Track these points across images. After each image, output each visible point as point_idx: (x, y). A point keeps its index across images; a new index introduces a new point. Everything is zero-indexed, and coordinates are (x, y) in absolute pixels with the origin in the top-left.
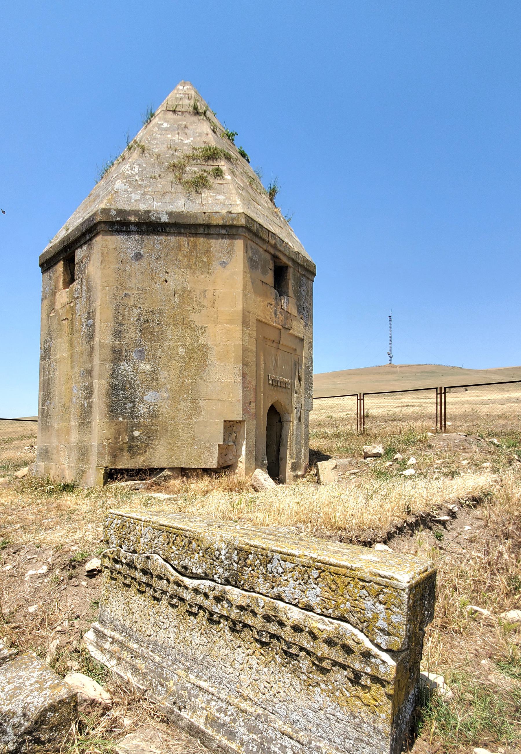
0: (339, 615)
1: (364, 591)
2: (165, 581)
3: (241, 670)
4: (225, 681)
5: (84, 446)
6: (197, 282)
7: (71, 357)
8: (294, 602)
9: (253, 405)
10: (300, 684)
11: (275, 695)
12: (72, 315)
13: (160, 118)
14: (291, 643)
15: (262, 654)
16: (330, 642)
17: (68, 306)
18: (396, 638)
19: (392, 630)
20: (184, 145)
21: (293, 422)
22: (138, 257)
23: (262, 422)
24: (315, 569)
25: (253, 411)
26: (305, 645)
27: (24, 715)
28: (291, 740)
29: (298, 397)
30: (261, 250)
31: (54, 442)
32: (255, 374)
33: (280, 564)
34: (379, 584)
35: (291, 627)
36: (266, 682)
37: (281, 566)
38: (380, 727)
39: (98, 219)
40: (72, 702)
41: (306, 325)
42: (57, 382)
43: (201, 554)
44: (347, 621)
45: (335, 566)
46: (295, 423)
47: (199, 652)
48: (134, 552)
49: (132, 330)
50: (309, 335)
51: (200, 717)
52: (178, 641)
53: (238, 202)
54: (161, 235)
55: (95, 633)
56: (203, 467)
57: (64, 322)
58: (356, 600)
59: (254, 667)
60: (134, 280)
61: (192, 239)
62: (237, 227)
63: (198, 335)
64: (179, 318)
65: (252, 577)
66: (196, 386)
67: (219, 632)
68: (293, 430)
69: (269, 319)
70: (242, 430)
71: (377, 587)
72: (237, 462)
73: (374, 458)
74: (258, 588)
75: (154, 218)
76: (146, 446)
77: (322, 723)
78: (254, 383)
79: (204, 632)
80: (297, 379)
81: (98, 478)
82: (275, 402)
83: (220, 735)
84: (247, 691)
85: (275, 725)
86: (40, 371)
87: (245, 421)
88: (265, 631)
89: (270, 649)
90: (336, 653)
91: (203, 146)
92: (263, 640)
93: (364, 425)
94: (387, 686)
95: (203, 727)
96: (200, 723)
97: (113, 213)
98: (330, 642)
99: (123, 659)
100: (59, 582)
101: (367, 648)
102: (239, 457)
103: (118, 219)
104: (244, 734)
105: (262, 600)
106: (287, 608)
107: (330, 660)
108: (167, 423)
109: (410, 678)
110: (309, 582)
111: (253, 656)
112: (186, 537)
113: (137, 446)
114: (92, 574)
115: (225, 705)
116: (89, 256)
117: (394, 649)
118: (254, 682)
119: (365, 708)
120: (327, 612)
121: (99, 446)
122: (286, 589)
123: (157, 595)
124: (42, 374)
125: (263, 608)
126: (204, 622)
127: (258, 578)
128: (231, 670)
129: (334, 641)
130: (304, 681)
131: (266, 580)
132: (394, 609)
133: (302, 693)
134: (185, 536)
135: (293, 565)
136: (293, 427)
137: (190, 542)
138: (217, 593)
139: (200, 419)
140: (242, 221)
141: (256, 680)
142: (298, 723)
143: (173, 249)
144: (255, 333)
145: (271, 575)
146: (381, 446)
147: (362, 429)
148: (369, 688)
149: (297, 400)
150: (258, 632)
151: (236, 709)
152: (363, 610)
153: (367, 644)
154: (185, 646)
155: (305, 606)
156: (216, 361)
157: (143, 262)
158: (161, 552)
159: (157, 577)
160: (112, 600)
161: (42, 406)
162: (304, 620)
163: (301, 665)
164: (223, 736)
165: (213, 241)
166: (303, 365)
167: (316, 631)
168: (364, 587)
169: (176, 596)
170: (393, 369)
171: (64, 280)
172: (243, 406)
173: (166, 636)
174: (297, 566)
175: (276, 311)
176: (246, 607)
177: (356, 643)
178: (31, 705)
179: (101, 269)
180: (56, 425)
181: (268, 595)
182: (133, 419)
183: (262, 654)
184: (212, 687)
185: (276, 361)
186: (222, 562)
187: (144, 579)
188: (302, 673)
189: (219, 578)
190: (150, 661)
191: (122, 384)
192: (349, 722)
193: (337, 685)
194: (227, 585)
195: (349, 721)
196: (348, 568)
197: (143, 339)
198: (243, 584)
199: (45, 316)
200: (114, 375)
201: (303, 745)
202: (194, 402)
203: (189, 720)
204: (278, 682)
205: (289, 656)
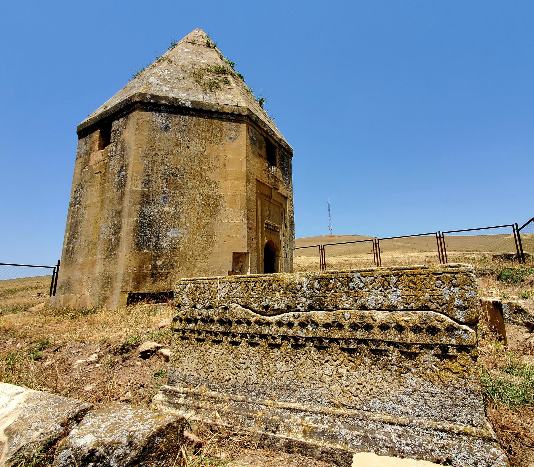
2: (245, 325)
3: (331, 382)
4: (315, 397)
5: (109, 275)
6: (213, 150)
7: (102, 202)
8: (378, 307)
11: (368, 393)
12: (106, 169)
13: (182, 46)
15: (351, 361)
16: (416, 329)
17: (102, 163)
19: (468, 304)
20: (200, 63)
22: (167, 129)
25: (254, 246)
26: (393, 339)
27: (130, 444)
28: (393, 426)
29: (285, 239)
30: (258, 133)
31: (78, 274)
33: (361, 280)
34: (450, 273)
35: (379, 327)
38: (472, 387)
39: (136, 99)
40: (180, 427)
41: (288, 188)
42: (85, 223)
43: (282, 292)
45: (411, 269)
47: (285, 379)
48: (210, 307)
52: (261, 376)
53: (242, 100)
54: (186, 115)
55: (165, 394)
57: (97, 175)
58: (434, 290)
59: (344, 375)
60: (162, 145)
61: (209, 120)
62: (242, 116)
64: (198, 174)
67: (305, 354)
69: (265, 180)
71: (449, 275)
75: (180, 104)
76: (168, 273)
77: (418, 403)
78: (255, 224)
80: (283, 225)
81: (121, 301)
84: (338, 399)
86: (69, 215)
88: (352, 339)
89: (358, 354)
91: (215, 65)
92: (351, 347)
95: (303, 440)
97: (148, 96)
98: (416, 329)
99: (202, 408)
100: (112, 365)
103: (152, 101)
104: (347, 434)
107: (418, 344)
110: (389, 287)
112: (265, 281)
114: (145, 355)
115: (319, 416)
116: (125, 126)
118: (345, 388)
123: (237, 339)
124: (70, 218)
125: (349, 319)
126: (289, 350)
127: (341, 297)
131: (349, 296)
132: (467, 288)
137: (270, 285)
138: (302, 319)
139: (214, 251)
140: (246, 112)
142: (395, 410)
143: (194, 125)
144: (255, 188)
145: (353, 291)
150: (345, 342)
152: (441, 296)
154: (269, 378)
155: (389, 307)
157: (171, 133)
158: (239, 301)
159: (236, 322)
160: (184, 358)
161: (68, 244)
163: (390, 358)
164: (326, 442)
165: (224, 123)
167: (403, 323)
168: (438, 279)
169: (258, 335)
170: (333, 238)
171: (100, 144)
173: (250, 373)
175: (268, 175)
178: (137, 433)
179: (136, 134)
180: (80, 260)
183: (351, 361)
185: (269, 211)
186: (304, 293)
187: (221, 329)
189: (302, 307)
190: (232, 402)
191: (149, 222)
192: (442, 393)
195: (443, 392)
199: (78, 171)
200: (142, 215)
201: (404, 426)
202: (209, 237)
203: (287, 439)
204: (369, 381)
205: (378, 354)
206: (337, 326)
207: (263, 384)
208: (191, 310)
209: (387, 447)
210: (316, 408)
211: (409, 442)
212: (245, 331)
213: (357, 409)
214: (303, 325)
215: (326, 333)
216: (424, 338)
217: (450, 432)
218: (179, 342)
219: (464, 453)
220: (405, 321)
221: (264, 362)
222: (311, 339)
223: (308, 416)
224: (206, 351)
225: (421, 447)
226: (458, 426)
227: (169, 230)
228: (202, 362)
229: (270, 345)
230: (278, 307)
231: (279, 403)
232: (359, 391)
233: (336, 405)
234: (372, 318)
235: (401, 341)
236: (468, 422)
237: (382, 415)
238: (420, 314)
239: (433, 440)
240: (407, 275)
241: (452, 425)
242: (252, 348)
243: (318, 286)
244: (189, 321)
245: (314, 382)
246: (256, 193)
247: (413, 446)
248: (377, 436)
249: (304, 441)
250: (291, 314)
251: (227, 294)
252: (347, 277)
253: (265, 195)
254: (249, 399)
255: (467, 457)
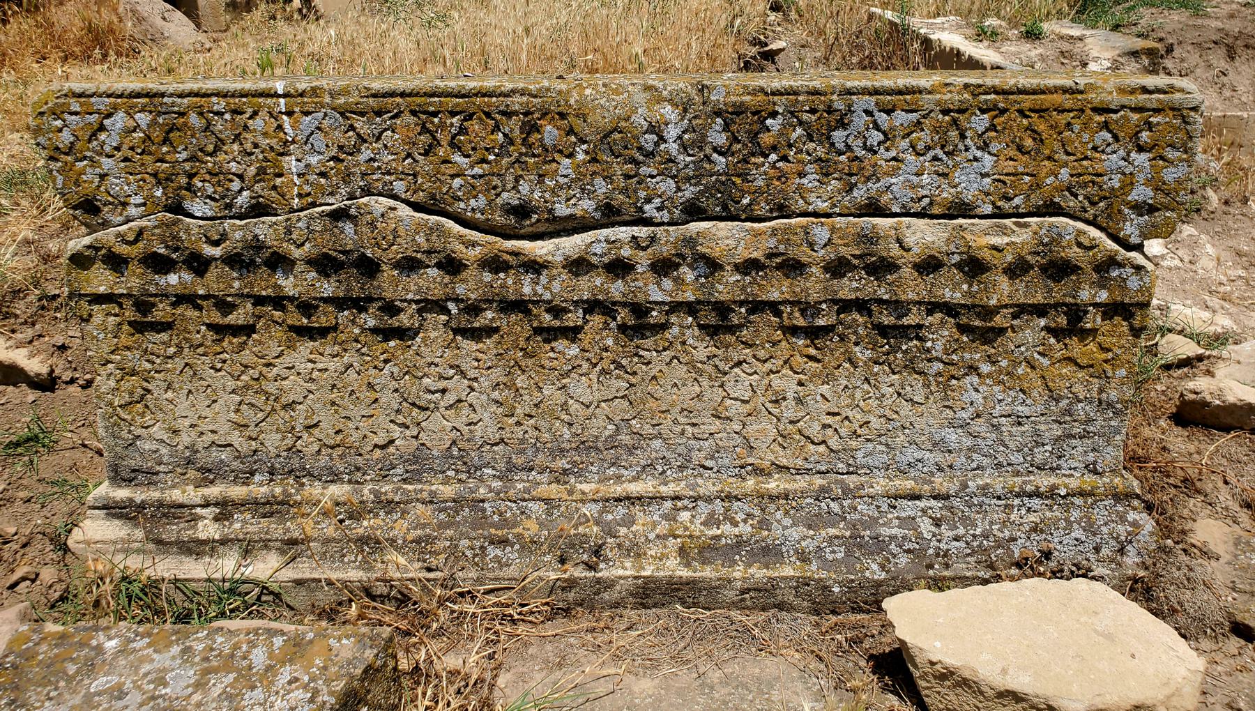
2: (433, 272)
3: (750, 415)
4: (697, 457)
8: (917, 208)
16: (1017, 270)
28: (917, 502)
34: (1138, 109)
43: (581, 157)
45: (1034, 92)
47: (599, 422)
48: (259, 210)
58: (1086, 158)
59: (790, 395)
65: (779, 179)
67: (665, 349)
74: (801, 201)
83: (741, 568)
84: (766, 455)
89: (836, 338)
95: (684, 573)
96: (674, 568)
98: (1017, 270)
112: (508, 114)
115: (718, 506)
118: (790, 427)
123: (405, 320)
126: (610, 342)
127: (801, 175)
131: (827, 175)
132: (1171, 154)
134: (503, 113)
135: (914, 117)
137: (531, 128)
138: (664, 249)
142: (920, 465)
145: (843, 158)
150: (803, 312)
152: (1101, 175)
154: (544, 425)
155: (949, 209)
158: (399, 187)
159: (397, 265)
163: (929, 344)
164: (750, 566)
167: (986, 255)
168: (1106, 126)
169: (490, 302)
176: (762, 259)
187: (328, 288)
194: (688, 222)
203: (636, 578)
204: (862, 403)
206: (779, 267)
207: (522, 441)
208: (162, 224)
209: (909, 551)
210: (707, 486)
211: (961, 531)
212: (438, 293)
213: (819, 472)
214: (663, 267)
215: (743, 288)
216: (1033, 291)
217: (1051, 493)
218: (124, 340)
219: (1078, 533)
220: (995, 248)
221: (521, 381)
222: (692, 308)
223: (686, 508)
224: (268, 365)
225: (987, 538)
226: (1067, 480)
228: (259, 400)
229: (538, 331)
230: (569, 211)
231: (585, 487)
232: (829, 432)
233: (762, 470)
234: (899, 241)
235: (969, 301)
236: (1086, 467)
237: (891, 480)
238: (1035, 227)
239: (1013, 517)
240: (1021, 112)
241: (1053, 480)
242: (469, 345)
243: (721, 139)
244: (160, 264)
245: (694, 421)
247: (970, 538)
248: (885, 531)
249: (690, 574)
250: (623, 233)
251: (335, 159)
252: (830, 110)
254: (482, 491)
255: (1083, 538)
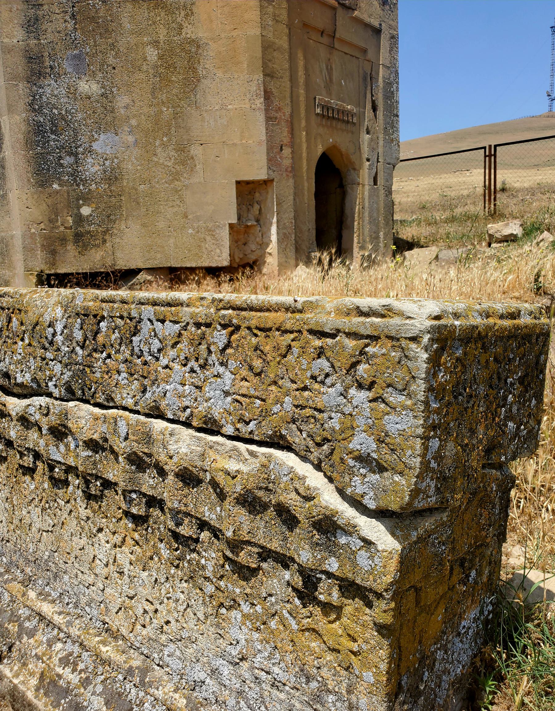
0: (270, 433)
1: (323, 363)
3: (106, 578)
9: (287, 151)
10: (204, 603)
14: (179, 512)
16: (251, 503)
18: (397, 478)
19: (388, 458)
21: (363, 185)
23: (306, 184)
24: (219, 327)
25: (287, 162)
29: (371, 140)
32: (288, 94)
33: (154, 330)
34: (353, 335)
35: (177, 475)
36: (147, 600)
37: (156, 335)
43: (27, 341)
44: (288, 448)
45: (260, 310)
46: (367, 187)
47: (41, 546)
49: (58, 17)
50: (391, 22)
51: (32, 674)
52: (12, 527)
56: (206, 264)
58: (305, 388)
63: (179, 20)
66: (183, 120)
68: (363, 199)
70: (269, 196)
71: (350, 343)
72: (263, 256)
73: (505, 244)
76: (105, 233)
78: (287, 110)
79: (47, 505)
80: (369, 106)
82: (329, 149)
84: (118, 622)
85: (156, 692)
87: (273, 180)
88: (135, 491)
90: (265, 527)
92: (134, 511)
93: (495, 200)
94: (375, 603)
95: (30, 695)
101: (326, 508)
102: (267, 245)
105: (126, 420)
106: (167, 433)
107: (255, 545)
108: (136, 190)
109: (464, 582)
111: (123, 548)
113: (89, 232)
115: (76, 649)
117: (394, 507)
118: (128, 601)
119: (329, 657)
120: (245, 430)
121: (24, 236)
122: (168, 387)
125: (126, 439)
126: (46, 485)
128: (91, 579)
129: (260, 498)
130: (211, 596)
132: (394, 398)
133: (208, 622)
136: (363, 194)
141: (131, 598)
145: (139, 361)
146: (518, 222)
147: (492, 209)
148: (339, 609)
149: (369, 144)
151: (94, 658)
152: (320, 411)
153: (330, 499)
154: (23, 537)
156: (215, 71)
162: (203, 456)
166: (381, 80)
167: (221, 478)
168: (320, 353)
172: (268, 153)
174: (185, 328)
177: (304, 497)
181: (138, 408)
182: (78, 185)
184: (60, 613)
185: (330, 70)
188: (205, 578)
191: (52, 121)
192: (298, 689)
193: (272, 605)
195: (298, 686)
196: (287, 309)
197: (78, 34)
198: (95, 393)
200: (35, 105)
202: (182, 149)
227: (96, 136)
246: (290, 27)
253: (315, 29)
